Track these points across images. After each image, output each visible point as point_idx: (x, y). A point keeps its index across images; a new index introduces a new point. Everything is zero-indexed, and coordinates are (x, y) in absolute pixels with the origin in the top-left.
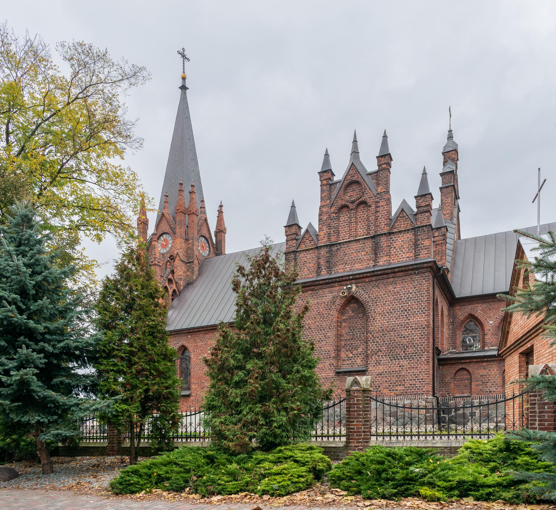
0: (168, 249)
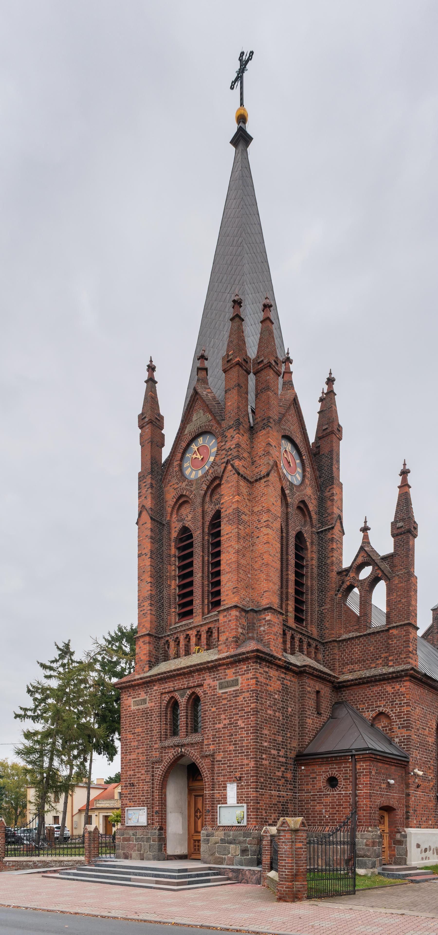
0: (207, 467)
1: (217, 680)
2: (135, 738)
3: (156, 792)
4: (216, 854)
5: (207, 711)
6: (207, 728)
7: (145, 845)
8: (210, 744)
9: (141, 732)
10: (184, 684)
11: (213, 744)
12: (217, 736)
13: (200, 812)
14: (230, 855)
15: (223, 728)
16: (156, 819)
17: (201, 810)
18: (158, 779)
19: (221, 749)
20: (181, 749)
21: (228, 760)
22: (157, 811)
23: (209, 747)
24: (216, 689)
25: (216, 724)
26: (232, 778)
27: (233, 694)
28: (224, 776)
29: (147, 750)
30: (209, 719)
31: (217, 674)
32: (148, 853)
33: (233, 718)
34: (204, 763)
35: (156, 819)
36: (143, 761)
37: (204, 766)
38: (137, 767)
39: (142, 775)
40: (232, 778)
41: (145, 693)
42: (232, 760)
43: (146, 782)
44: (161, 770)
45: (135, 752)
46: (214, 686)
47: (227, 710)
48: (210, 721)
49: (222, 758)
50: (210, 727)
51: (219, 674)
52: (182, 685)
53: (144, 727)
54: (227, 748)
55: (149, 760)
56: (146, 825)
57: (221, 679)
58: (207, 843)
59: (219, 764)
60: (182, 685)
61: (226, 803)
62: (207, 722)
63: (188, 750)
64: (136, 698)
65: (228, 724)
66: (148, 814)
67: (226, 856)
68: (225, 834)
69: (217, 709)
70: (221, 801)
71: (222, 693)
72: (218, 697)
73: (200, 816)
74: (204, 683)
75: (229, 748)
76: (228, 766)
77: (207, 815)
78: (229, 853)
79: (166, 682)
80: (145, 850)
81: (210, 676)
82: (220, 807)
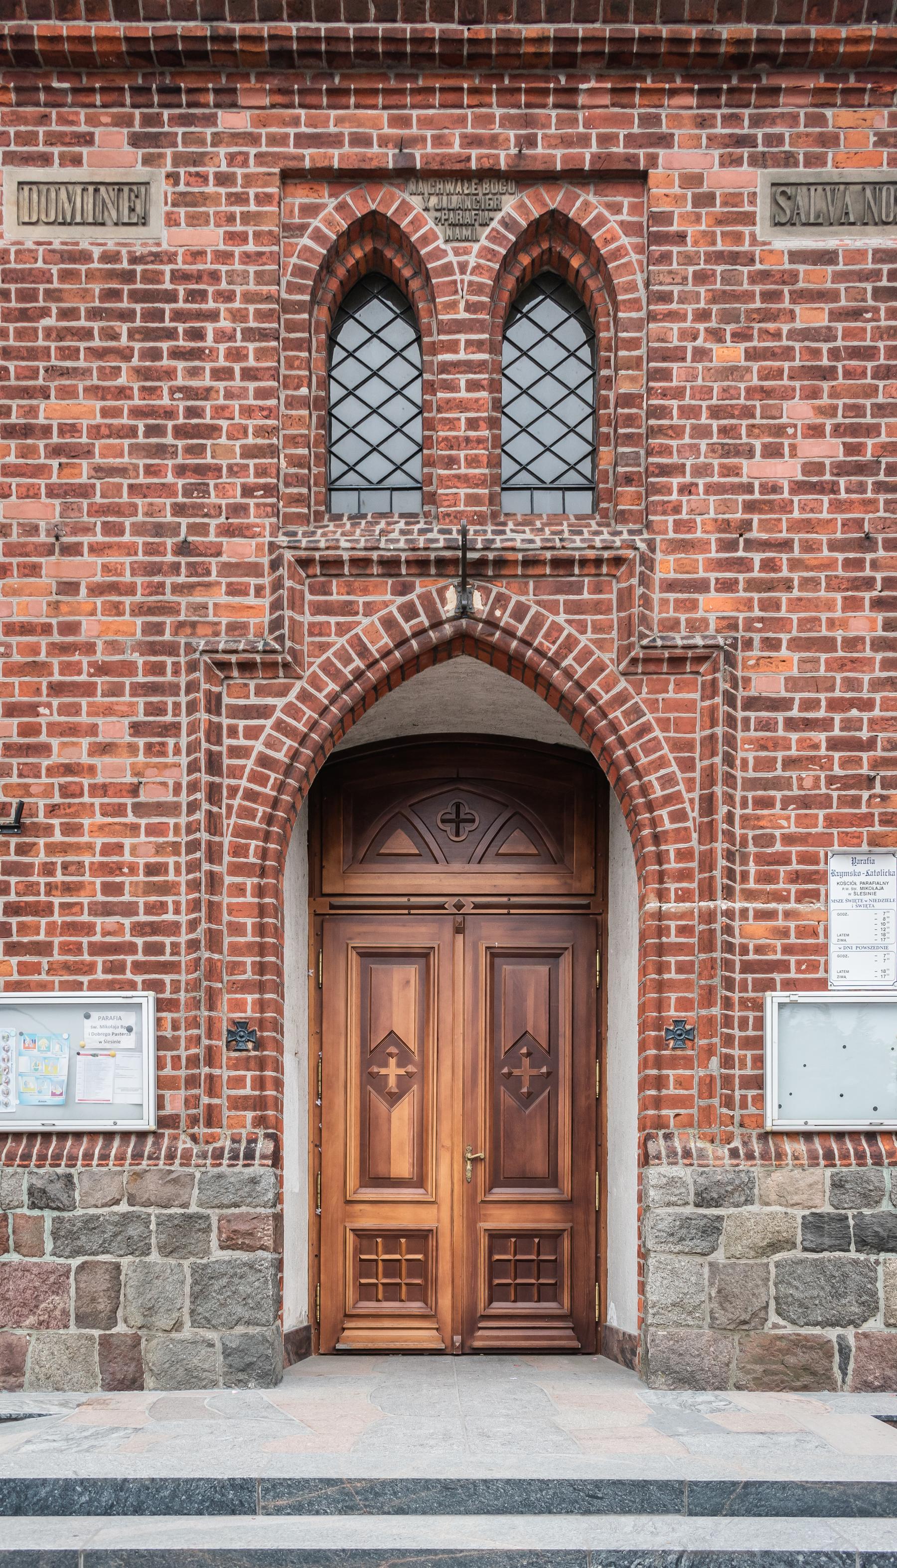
1: (759, 161)
2: (40, 471)
3: (240, 890)
4: (773, 1318)
5: (677, 355)
6: (679, 469)
7: (149, 1277)
8: (702, 586)
9: (96, 432)
10: (494, 141)
11: (727, 586)
12: (755, 534)
13: (404, 1058)
14: (875, 1325)
15: (798, 487)
16: (238, 1082)
17: (413, 1044)
18: (250, 795)
19: (782, 624)
20: (463, 589)
21: (834, 705)
22: (242, 1025)
23: (693, 605)
24: (749, 219)
25: (750, 453)
26: (867, 819)
27: (875, 275)
28: (805, 802)
29: (152, 569)
30: (689, 412)
31: (756, 122)
32: (187, 1332)
33: (872, 430)
34: (653, 705)
35: (238, 1082)
36: (113, 647)
37: (645, 729)
38: (56, 689)
39: (105, 749)
40: (867, 819)
41: (136, 141)
42: (868, 705)
43: (139, 809)
44: (279, 726)
45: (34, 570)
46: (732, 199)
47: (828, 374)
48: (702, 432)
49: (793, 684)
50: (702, 470)
51: (773, 120)
52: (471, 141)
53: (123, 393)
54: (831, 623)
55: (171, 649)
56: (148, 1122)
57: (789, 160)
58: (703, 1245)
59: (766, 725)
60: (471, 141)
61: (823, 984)
62: (678, 432)
63: (520, 612)
64: (45, 160)
65: (841, 469)
66: (162, 1043)
67: (850, 1333)
68: (838, 1184)
69: (751, 355)
70: (783, 966)
71: (796, 256)
72: (765, 276)
73: (404, 1083)
74: (653, 160)
75: (844, 624)
76: (834, 744)
77: (673, 1063)
78: (871, 1308)
79: (337, 95)
80: (150, 1311)
81: (703, 122)
82: (781, 1006)
